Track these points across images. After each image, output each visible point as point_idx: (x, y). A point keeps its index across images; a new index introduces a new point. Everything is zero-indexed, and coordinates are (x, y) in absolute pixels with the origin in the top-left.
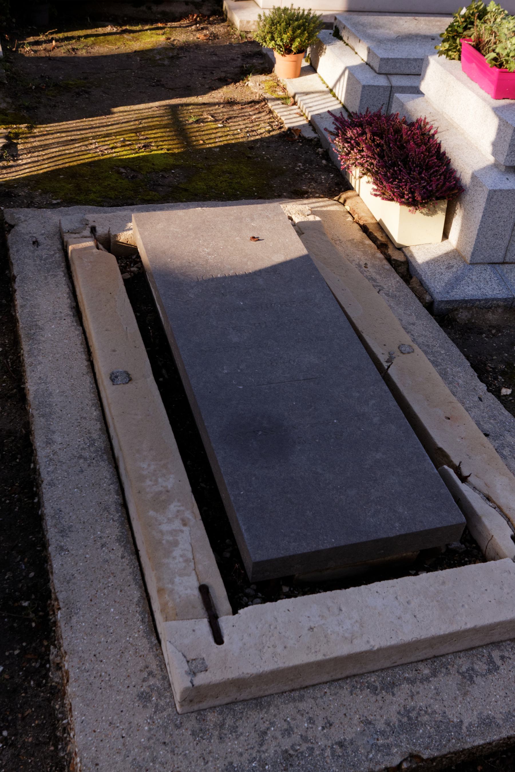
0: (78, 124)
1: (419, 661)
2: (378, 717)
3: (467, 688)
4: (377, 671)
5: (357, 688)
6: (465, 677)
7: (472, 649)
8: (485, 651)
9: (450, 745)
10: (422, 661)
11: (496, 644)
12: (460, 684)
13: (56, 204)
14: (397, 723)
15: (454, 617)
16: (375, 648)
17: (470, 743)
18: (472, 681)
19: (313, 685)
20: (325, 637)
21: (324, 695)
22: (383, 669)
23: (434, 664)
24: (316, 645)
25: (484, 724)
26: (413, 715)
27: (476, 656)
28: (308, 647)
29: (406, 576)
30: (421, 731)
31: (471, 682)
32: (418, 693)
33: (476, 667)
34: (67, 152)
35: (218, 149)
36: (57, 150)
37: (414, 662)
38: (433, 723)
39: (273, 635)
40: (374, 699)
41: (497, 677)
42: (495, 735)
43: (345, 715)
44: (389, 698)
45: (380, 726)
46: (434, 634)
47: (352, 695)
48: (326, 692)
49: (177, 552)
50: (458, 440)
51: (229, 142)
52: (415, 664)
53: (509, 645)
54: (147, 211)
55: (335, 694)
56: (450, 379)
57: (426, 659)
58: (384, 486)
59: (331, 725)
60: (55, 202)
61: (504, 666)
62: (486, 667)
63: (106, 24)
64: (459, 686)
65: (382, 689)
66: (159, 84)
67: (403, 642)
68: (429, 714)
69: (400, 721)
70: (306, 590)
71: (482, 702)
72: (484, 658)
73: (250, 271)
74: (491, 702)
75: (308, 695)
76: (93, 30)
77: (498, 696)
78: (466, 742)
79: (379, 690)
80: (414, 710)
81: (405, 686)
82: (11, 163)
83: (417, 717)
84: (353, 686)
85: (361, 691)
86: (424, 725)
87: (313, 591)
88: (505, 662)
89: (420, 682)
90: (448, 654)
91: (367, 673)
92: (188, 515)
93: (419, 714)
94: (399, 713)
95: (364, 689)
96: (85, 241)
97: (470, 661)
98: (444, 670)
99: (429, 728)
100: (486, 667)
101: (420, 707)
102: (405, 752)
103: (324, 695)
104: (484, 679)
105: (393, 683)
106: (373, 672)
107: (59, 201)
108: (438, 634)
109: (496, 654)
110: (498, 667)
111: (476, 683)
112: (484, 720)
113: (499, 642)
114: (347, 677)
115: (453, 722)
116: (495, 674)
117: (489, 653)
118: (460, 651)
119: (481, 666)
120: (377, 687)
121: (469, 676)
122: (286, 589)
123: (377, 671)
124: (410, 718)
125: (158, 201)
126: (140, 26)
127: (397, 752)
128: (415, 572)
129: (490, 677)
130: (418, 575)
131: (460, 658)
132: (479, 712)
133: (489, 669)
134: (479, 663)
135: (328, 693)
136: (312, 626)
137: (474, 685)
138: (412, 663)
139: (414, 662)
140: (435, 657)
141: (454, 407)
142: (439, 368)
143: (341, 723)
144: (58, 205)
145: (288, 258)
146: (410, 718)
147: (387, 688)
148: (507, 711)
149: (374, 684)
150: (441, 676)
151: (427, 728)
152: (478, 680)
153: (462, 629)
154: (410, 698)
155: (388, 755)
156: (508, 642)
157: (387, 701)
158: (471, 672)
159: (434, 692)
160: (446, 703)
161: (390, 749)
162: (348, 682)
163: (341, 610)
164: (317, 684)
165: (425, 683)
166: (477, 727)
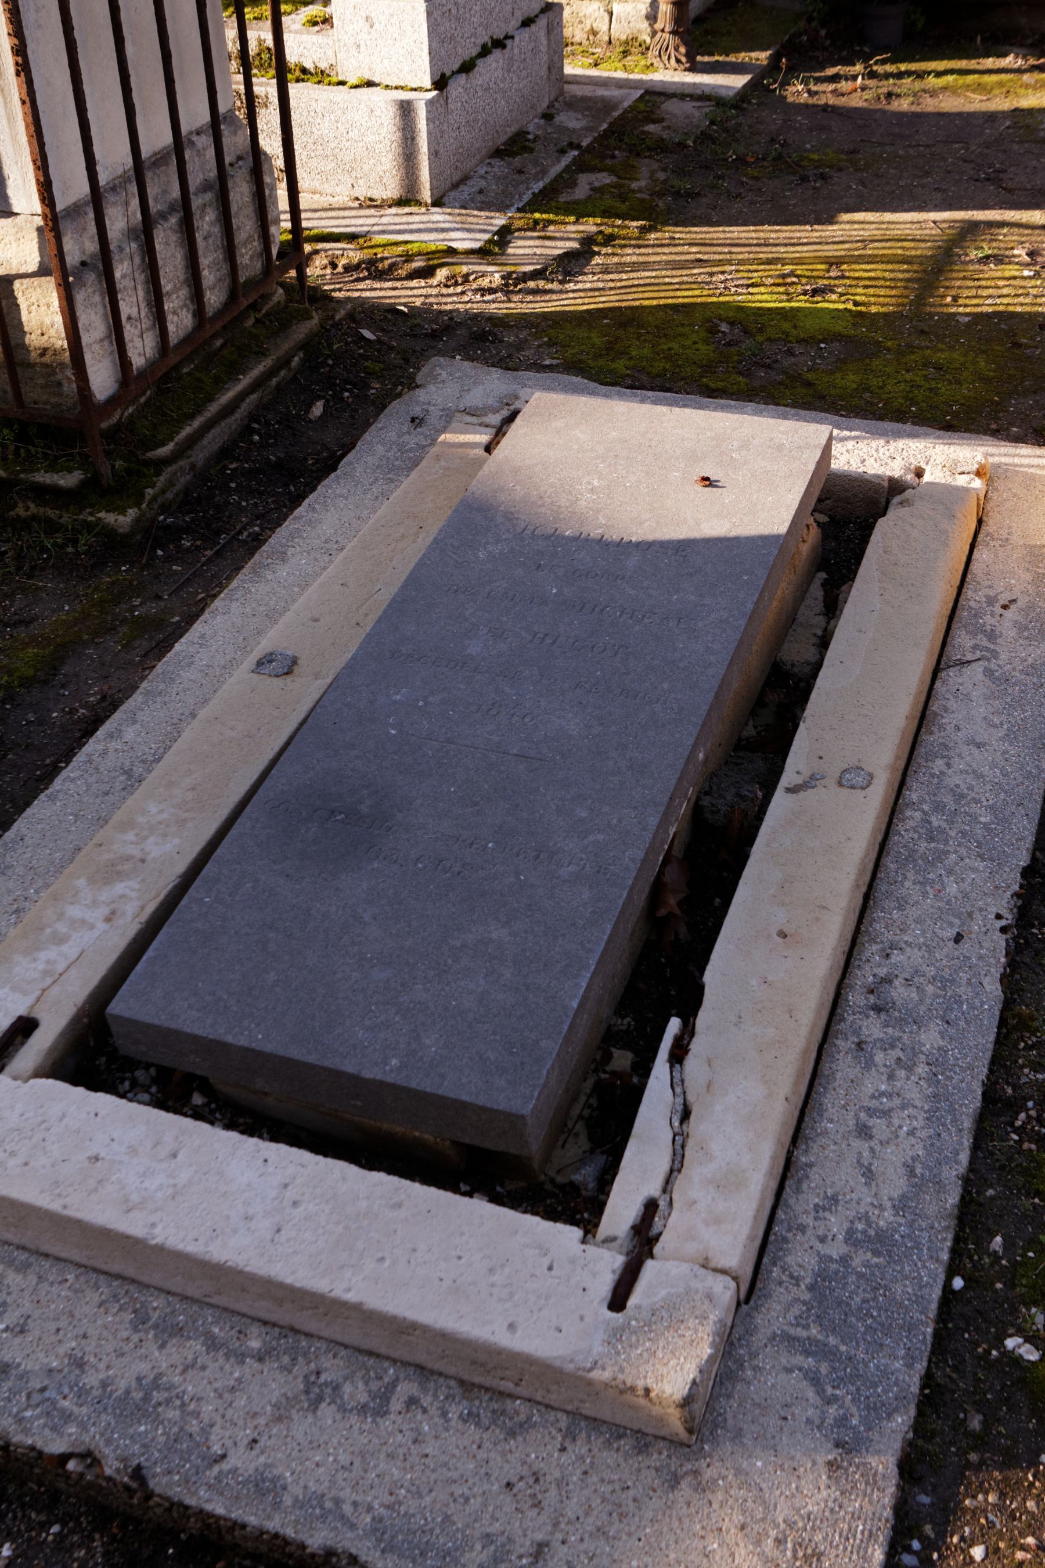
0: (743, 235)
1: (259, 1320)
2: (102, 1366)
3: (294, 1412)
4: (174, 1294)
5: (118, 1301)
6: (307, 1392)
7: (370, 1353)
8: (392, 1371)
9: (165, 1480)
10: (265, 1323)
11: (423, 1372)
12: (287, 1398)
13: (547, 366)
14: (120, 1392)
15: (342, 1267)
16: (154, 1242)
17: (199, 1498)
18: (314, 1405)
19: (58, 1259)
20: (100, 1182)
21: (60, 1283)
22: (187, 1298)
23: (279, 1339)
24: (71, 1185)
25: (257, 1485)
26: (157, 1396)
27: (368, 1371)
28: (57, 1182)
29: (107, 1092)
30: (143, 1428)
31: (310, 1406)
32: (203, 1368)
33: (347, 1388)
34: (667, 280)
35: (967, 319)
36: (654, 274)
37: (249, 1317)
38: (175, 1429)
39: (31, 1138)
40: (125, 1334)
41: (365, 1427)
42: (256, 1515)
43: (58, 1330)
44: (151, 1347)
45: (91, 1379)
46: (273, 1274)
47: (99, 1307)
48: (66, 1280)
49: (50, 953)
50: (754, 982)
51: (1011, 309)
52: (249, 1321)
53: (449, 1387)
54: (606, 396)
55: (76, 1291)
56: (931, 876)
57: (274, 1325)
58: (447, 988)
59: (22, 1332)
60: (547, 362)
61: (399, 1419)
62: (363, 1397)
63: (1008, 48)
64: (284, 1400)
65: (156, 1327)
66: (995, 179)
67: (207, 1257)
68: (183, 1412)
69: (128, 1392)
70: (241, 1120)
71: (293, 1449)
72: (379, 1383)
73: (634, 539)
74: (307, 1459)
75: (37, 1269)
76: (973, 62)
77: (331, 1459)
78: (195, 1493)
79: (147, 1326)
80: (168, 1389)
81: (196, 1346)
82: (555, 286)
83: (160, 1404)
84: (115, 1296)
85: (120, 1309)
86: (157, 1421)
87: (249, 1131)
88: (408, 1411)
89: (226, 1354)
90: (320, 1338)
91: (155, 1288)
92: (130, 909)
93: (168, 1401)
94: (139, 1379)
95: (126, 1310)
96: (475, 433)
97: (347, 1371)
98: (286, 1360)
99: (160, 1432)
100: (363, 1397)
101: (184, 1392)
102: (83, 1443)
103: (60, 1283)
104: (339, 1416)
105: (181, 1329)
106: (169, 1293)
107: (555, 362)
108: (280, 1279)
109: (406, 1388)
110: (387, 1413)
111: (319, 1413)
112: (263, 1481)
113: (432, 1372)
114: (118, 1277)
115: (209, 1448)
116: (369, 1420)
117: (397, 1379)
118: (346, 1347)
119: (356, 1392)
120: (149, 1319)
121: (315, 1394)
122: (198, 1099)
123: (174, 1294)
124: (146, 1398)
125: (733, 394)
126: (1010, 58)
127: (70, 1435)
128: (468, 1188)
129: (354, 1419)
130: (471, 1196)
131: (335, 1356)
132: (269, 1461)
133: (365, 1406)
134: (360, 1385)
135: (68, 1284)
136: (102, 1155)
137: (310, 1416)
138: (244, 1315)
139: (249, 1317)
140: (292, 1329)
141: (818, 919)
142: (933, 845)
143: (40, 1339)
144: (550, 368)
145: (733, 533)
146: (146, 1398)
147: (163, 1331)
148: (319, 1492)
149: (151, 1312)
150: (270, 1366)
151: (157, 1429)
152: (327, 1412)
153: (332, 1294)
154: (180, 1368)
155: (54, 1429)
156: (453, 1383)
157: (143, 1350)
158: (329, 1391)
159: (232, 1383)
160: (230, 1411)
161: (66, 1423)
162: (114, 1284)
163: (174, 1156)
164: (65, 1260)
165: (232, 1359)
166: (239, 1483)
